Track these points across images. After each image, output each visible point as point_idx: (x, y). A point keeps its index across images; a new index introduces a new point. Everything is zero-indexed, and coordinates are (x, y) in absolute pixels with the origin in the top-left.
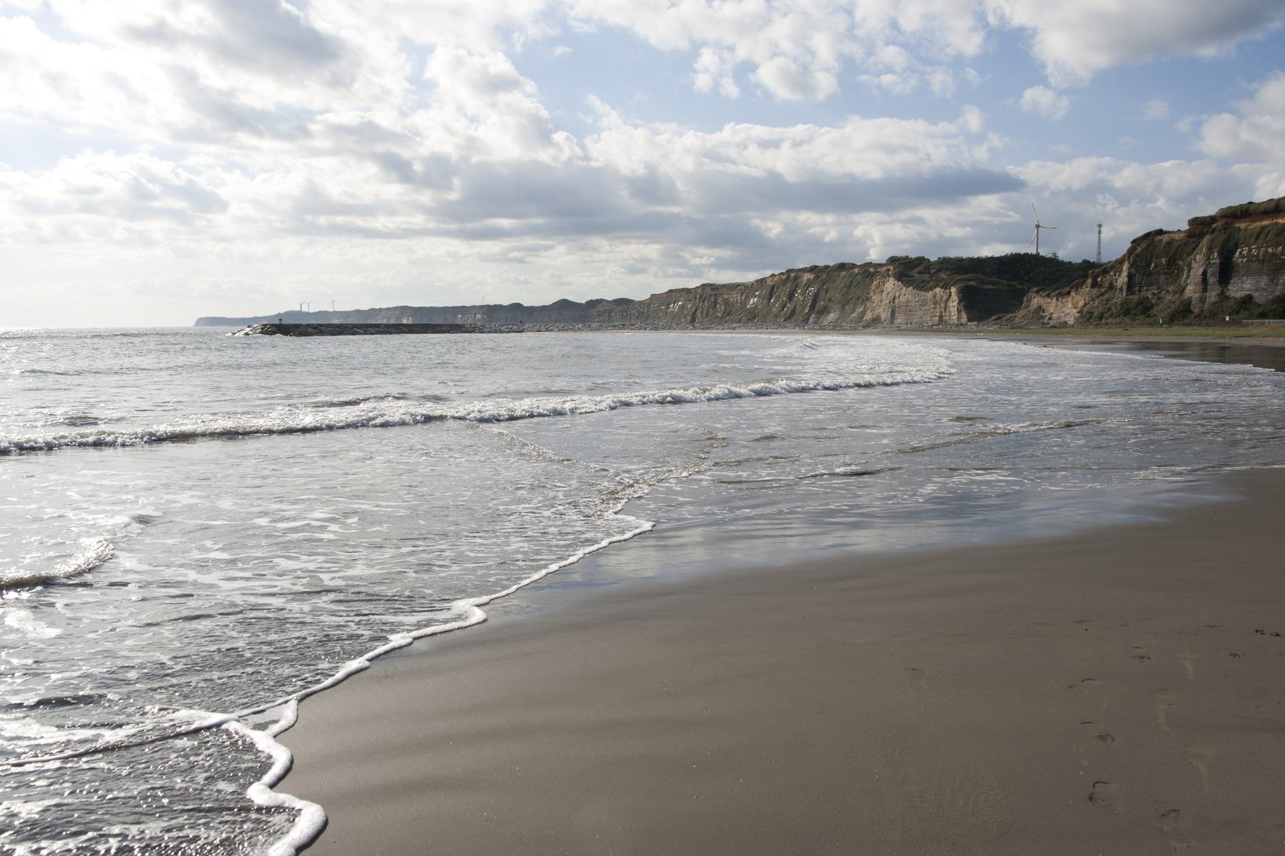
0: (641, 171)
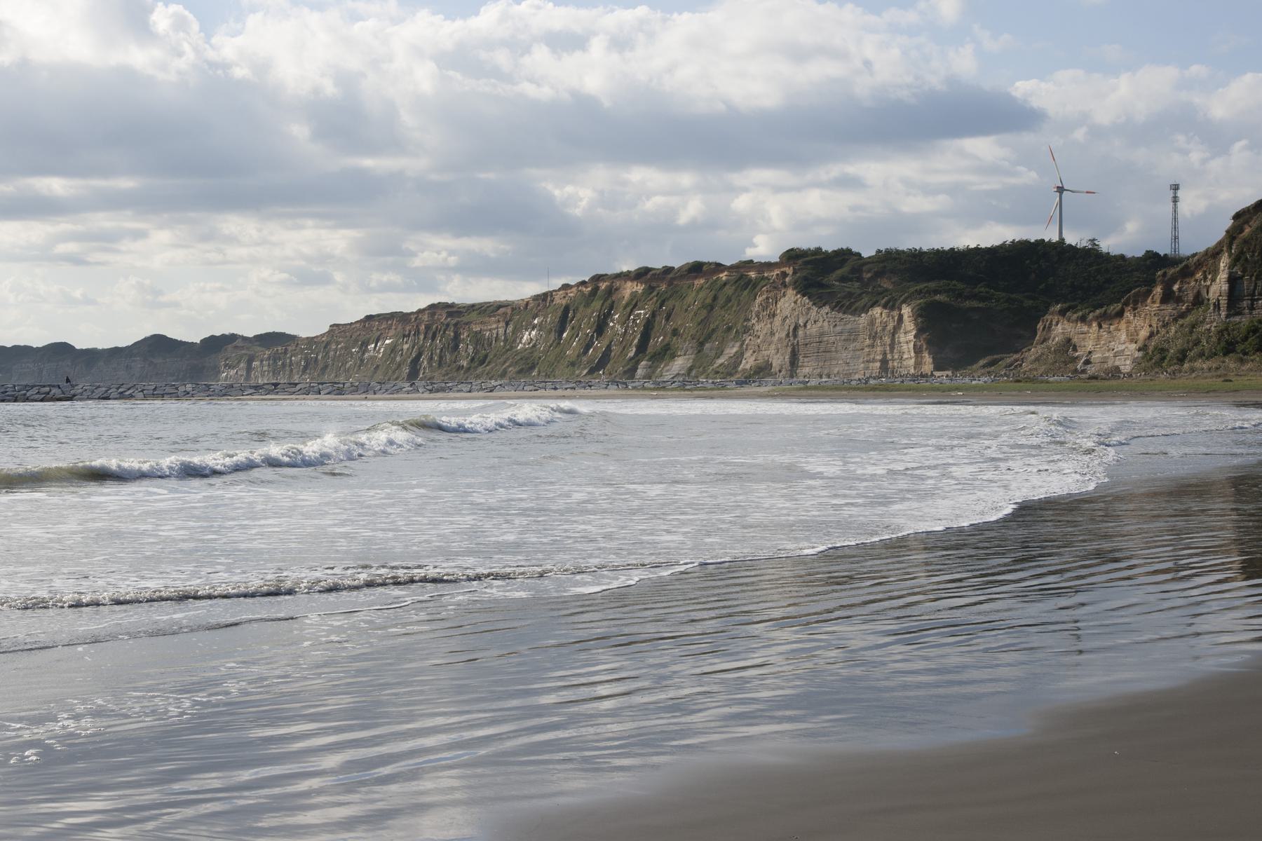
0: (330, 89)
